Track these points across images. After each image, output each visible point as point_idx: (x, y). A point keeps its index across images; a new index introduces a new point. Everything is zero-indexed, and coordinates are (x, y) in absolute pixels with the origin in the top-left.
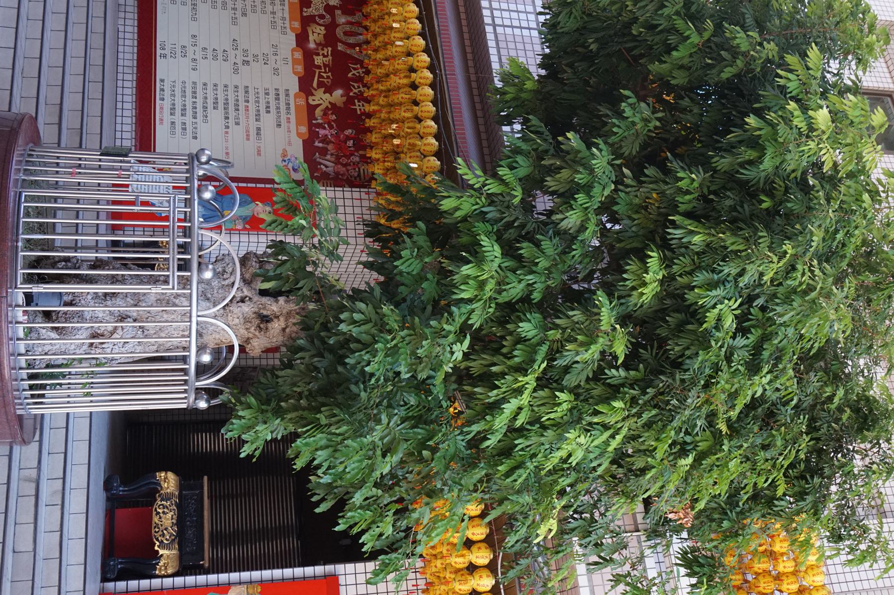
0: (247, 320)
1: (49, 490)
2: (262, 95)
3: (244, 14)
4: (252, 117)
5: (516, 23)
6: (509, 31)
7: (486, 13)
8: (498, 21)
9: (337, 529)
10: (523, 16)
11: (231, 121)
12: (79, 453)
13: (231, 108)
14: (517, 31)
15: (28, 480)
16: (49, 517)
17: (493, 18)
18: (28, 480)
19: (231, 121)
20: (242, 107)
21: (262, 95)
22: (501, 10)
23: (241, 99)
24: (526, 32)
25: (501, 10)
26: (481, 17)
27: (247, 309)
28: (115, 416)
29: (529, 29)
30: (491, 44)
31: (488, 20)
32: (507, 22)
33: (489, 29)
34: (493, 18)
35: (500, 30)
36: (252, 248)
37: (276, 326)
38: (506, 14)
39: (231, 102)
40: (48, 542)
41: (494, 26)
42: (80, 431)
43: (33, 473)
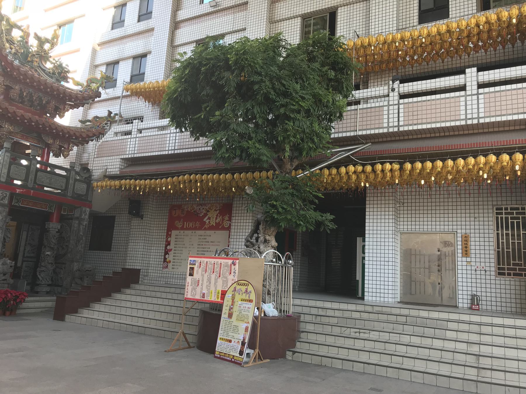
0: (266, 247)
1: (321, 312)
2: (201, 240)
3: (184, 244)
4: (208, 243)
5: (174, 141)
6: (177, 144)
7: (170, 152)
8: (173, 148)
9: (334, 217)
10: (171, 138)
11: (209, 250)
12: (305, 302)
13: (204, 250)
14: (177, 141)
15: (316, 318)
16: (330, 313)
17: (172, 150)
18: (316, 318)
19: (209, 250)
20: (204, 247)
21: (201, 240)
22: (169, 147)
23: (202, 246)
24: (177, 138)
25: (169, 147)
26: (171, 154)
27: (262, 247)
28: (110, 251)
29: (176, 136)
30: (181, 151)
31: (173, 152)
32: (173, 145)
33: (176, 152)
34: (172, 150)
35: (176, 148)
36: (243, 244)
37: (268, 237)
38: (171, 145)
39: (203, 249)
40: (337, 313)
41: (175, 150)
42: (298, 302)
43: (314, 316)
